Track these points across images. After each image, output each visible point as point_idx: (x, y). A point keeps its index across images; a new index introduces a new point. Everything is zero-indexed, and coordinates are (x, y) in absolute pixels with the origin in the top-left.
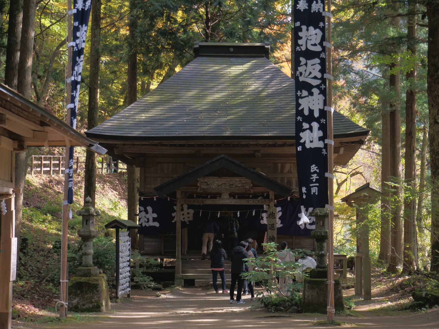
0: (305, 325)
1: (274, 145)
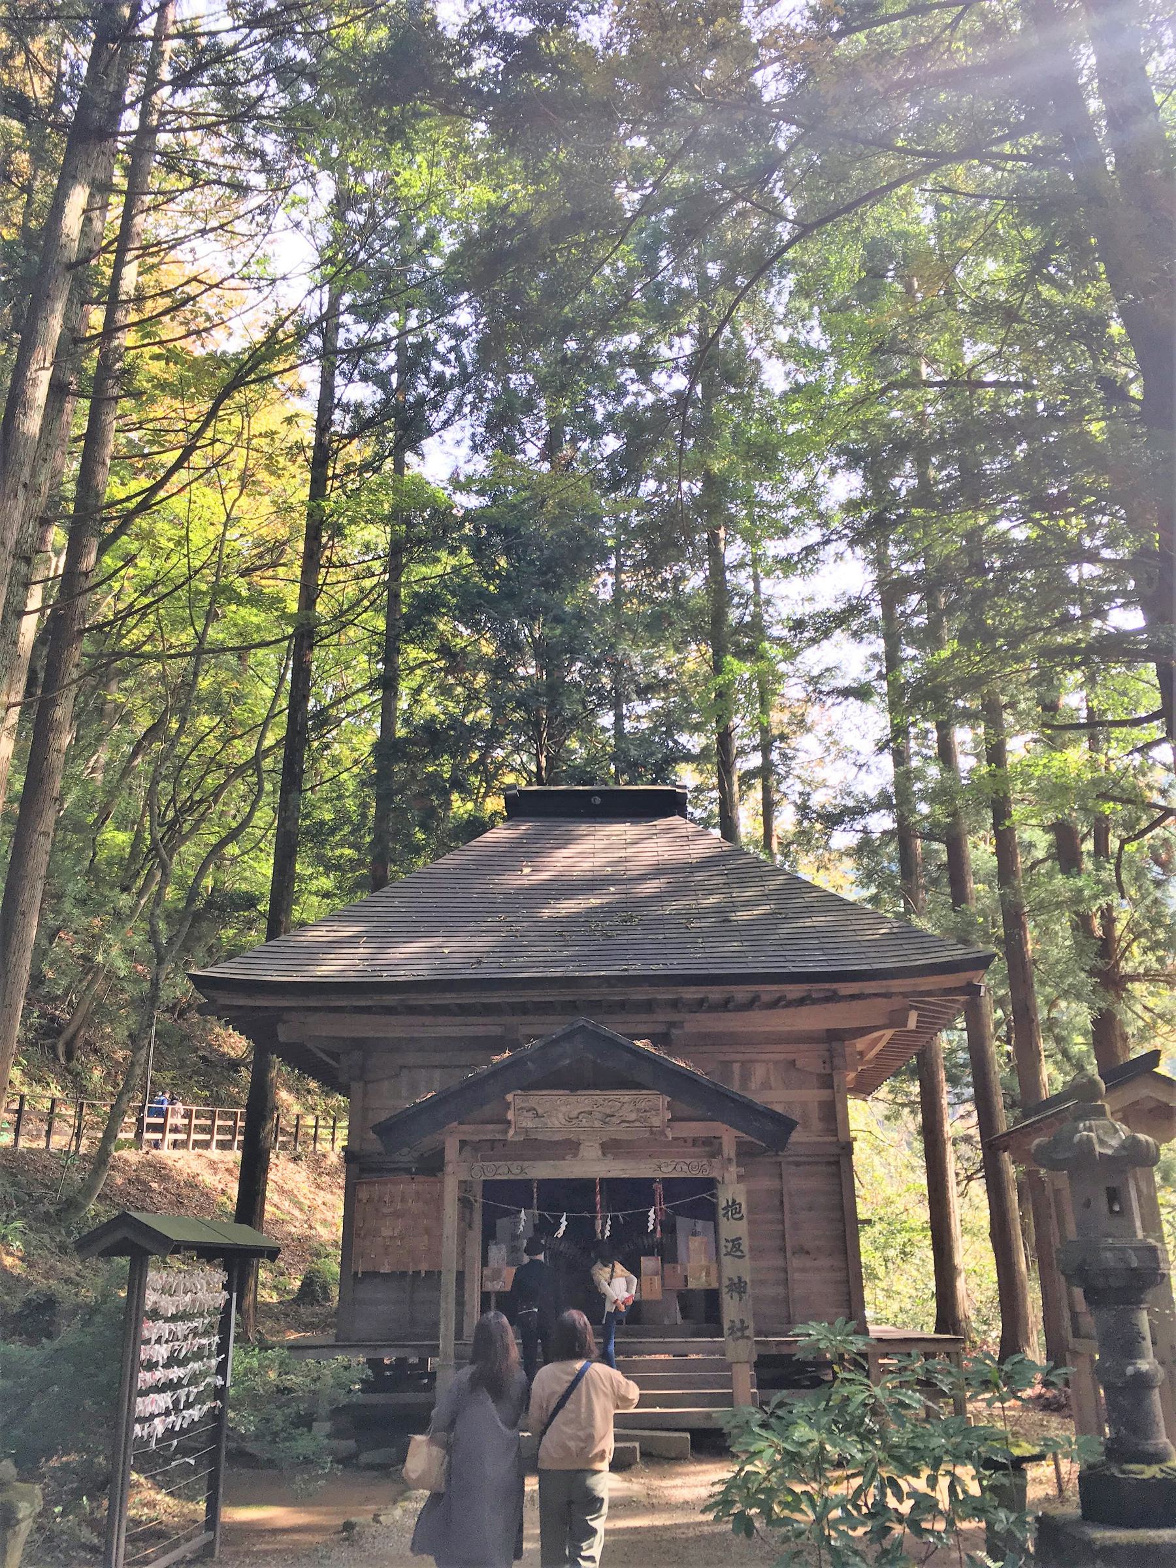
0: (312, 1002)
1: (725, 1005)
